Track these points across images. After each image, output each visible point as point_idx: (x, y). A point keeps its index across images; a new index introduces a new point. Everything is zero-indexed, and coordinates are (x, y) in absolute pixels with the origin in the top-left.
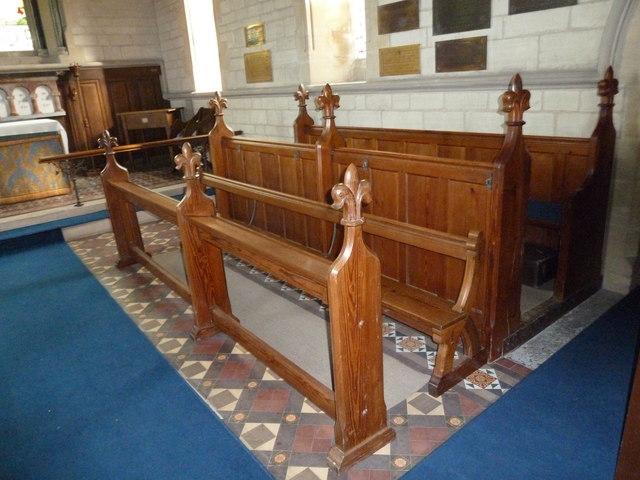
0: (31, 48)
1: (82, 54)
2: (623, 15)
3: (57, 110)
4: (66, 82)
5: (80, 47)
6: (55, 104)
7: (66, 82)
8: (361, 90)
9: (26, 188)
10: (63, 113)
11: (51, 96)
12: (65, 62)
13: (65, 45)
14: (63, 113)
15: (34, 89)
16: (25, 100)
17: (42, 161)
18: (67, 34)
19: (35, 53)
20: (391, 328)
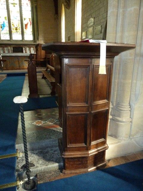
0: (32, 40)
1: (41, 42)
2: (120, 22)
3: (34, 53)
4: (37, 47)
5: (41, 40)
6: (34, 51)
7: (37, 47)
8: (21, 9)
9: (23, 66)
10: (36, 53)
11: (34, 50)
12: (38, 43)
13: (38, 39)
14: (36, 53)
15: (31, 48)
16: (29, 50)
17: (25, 61)
18: (39, 37)
19: (33, 41)
20: (37, 67)
